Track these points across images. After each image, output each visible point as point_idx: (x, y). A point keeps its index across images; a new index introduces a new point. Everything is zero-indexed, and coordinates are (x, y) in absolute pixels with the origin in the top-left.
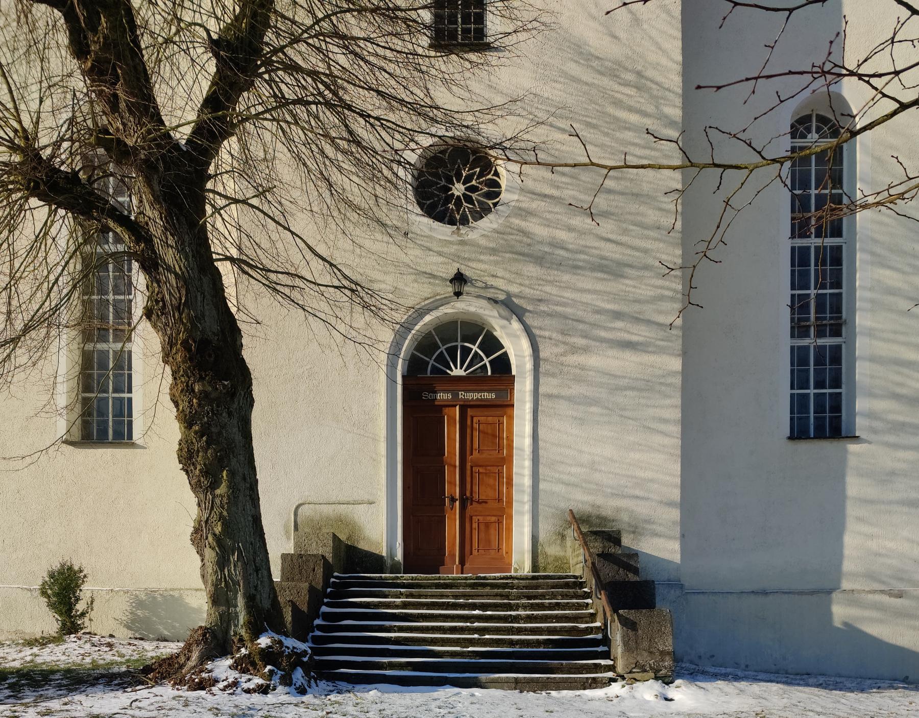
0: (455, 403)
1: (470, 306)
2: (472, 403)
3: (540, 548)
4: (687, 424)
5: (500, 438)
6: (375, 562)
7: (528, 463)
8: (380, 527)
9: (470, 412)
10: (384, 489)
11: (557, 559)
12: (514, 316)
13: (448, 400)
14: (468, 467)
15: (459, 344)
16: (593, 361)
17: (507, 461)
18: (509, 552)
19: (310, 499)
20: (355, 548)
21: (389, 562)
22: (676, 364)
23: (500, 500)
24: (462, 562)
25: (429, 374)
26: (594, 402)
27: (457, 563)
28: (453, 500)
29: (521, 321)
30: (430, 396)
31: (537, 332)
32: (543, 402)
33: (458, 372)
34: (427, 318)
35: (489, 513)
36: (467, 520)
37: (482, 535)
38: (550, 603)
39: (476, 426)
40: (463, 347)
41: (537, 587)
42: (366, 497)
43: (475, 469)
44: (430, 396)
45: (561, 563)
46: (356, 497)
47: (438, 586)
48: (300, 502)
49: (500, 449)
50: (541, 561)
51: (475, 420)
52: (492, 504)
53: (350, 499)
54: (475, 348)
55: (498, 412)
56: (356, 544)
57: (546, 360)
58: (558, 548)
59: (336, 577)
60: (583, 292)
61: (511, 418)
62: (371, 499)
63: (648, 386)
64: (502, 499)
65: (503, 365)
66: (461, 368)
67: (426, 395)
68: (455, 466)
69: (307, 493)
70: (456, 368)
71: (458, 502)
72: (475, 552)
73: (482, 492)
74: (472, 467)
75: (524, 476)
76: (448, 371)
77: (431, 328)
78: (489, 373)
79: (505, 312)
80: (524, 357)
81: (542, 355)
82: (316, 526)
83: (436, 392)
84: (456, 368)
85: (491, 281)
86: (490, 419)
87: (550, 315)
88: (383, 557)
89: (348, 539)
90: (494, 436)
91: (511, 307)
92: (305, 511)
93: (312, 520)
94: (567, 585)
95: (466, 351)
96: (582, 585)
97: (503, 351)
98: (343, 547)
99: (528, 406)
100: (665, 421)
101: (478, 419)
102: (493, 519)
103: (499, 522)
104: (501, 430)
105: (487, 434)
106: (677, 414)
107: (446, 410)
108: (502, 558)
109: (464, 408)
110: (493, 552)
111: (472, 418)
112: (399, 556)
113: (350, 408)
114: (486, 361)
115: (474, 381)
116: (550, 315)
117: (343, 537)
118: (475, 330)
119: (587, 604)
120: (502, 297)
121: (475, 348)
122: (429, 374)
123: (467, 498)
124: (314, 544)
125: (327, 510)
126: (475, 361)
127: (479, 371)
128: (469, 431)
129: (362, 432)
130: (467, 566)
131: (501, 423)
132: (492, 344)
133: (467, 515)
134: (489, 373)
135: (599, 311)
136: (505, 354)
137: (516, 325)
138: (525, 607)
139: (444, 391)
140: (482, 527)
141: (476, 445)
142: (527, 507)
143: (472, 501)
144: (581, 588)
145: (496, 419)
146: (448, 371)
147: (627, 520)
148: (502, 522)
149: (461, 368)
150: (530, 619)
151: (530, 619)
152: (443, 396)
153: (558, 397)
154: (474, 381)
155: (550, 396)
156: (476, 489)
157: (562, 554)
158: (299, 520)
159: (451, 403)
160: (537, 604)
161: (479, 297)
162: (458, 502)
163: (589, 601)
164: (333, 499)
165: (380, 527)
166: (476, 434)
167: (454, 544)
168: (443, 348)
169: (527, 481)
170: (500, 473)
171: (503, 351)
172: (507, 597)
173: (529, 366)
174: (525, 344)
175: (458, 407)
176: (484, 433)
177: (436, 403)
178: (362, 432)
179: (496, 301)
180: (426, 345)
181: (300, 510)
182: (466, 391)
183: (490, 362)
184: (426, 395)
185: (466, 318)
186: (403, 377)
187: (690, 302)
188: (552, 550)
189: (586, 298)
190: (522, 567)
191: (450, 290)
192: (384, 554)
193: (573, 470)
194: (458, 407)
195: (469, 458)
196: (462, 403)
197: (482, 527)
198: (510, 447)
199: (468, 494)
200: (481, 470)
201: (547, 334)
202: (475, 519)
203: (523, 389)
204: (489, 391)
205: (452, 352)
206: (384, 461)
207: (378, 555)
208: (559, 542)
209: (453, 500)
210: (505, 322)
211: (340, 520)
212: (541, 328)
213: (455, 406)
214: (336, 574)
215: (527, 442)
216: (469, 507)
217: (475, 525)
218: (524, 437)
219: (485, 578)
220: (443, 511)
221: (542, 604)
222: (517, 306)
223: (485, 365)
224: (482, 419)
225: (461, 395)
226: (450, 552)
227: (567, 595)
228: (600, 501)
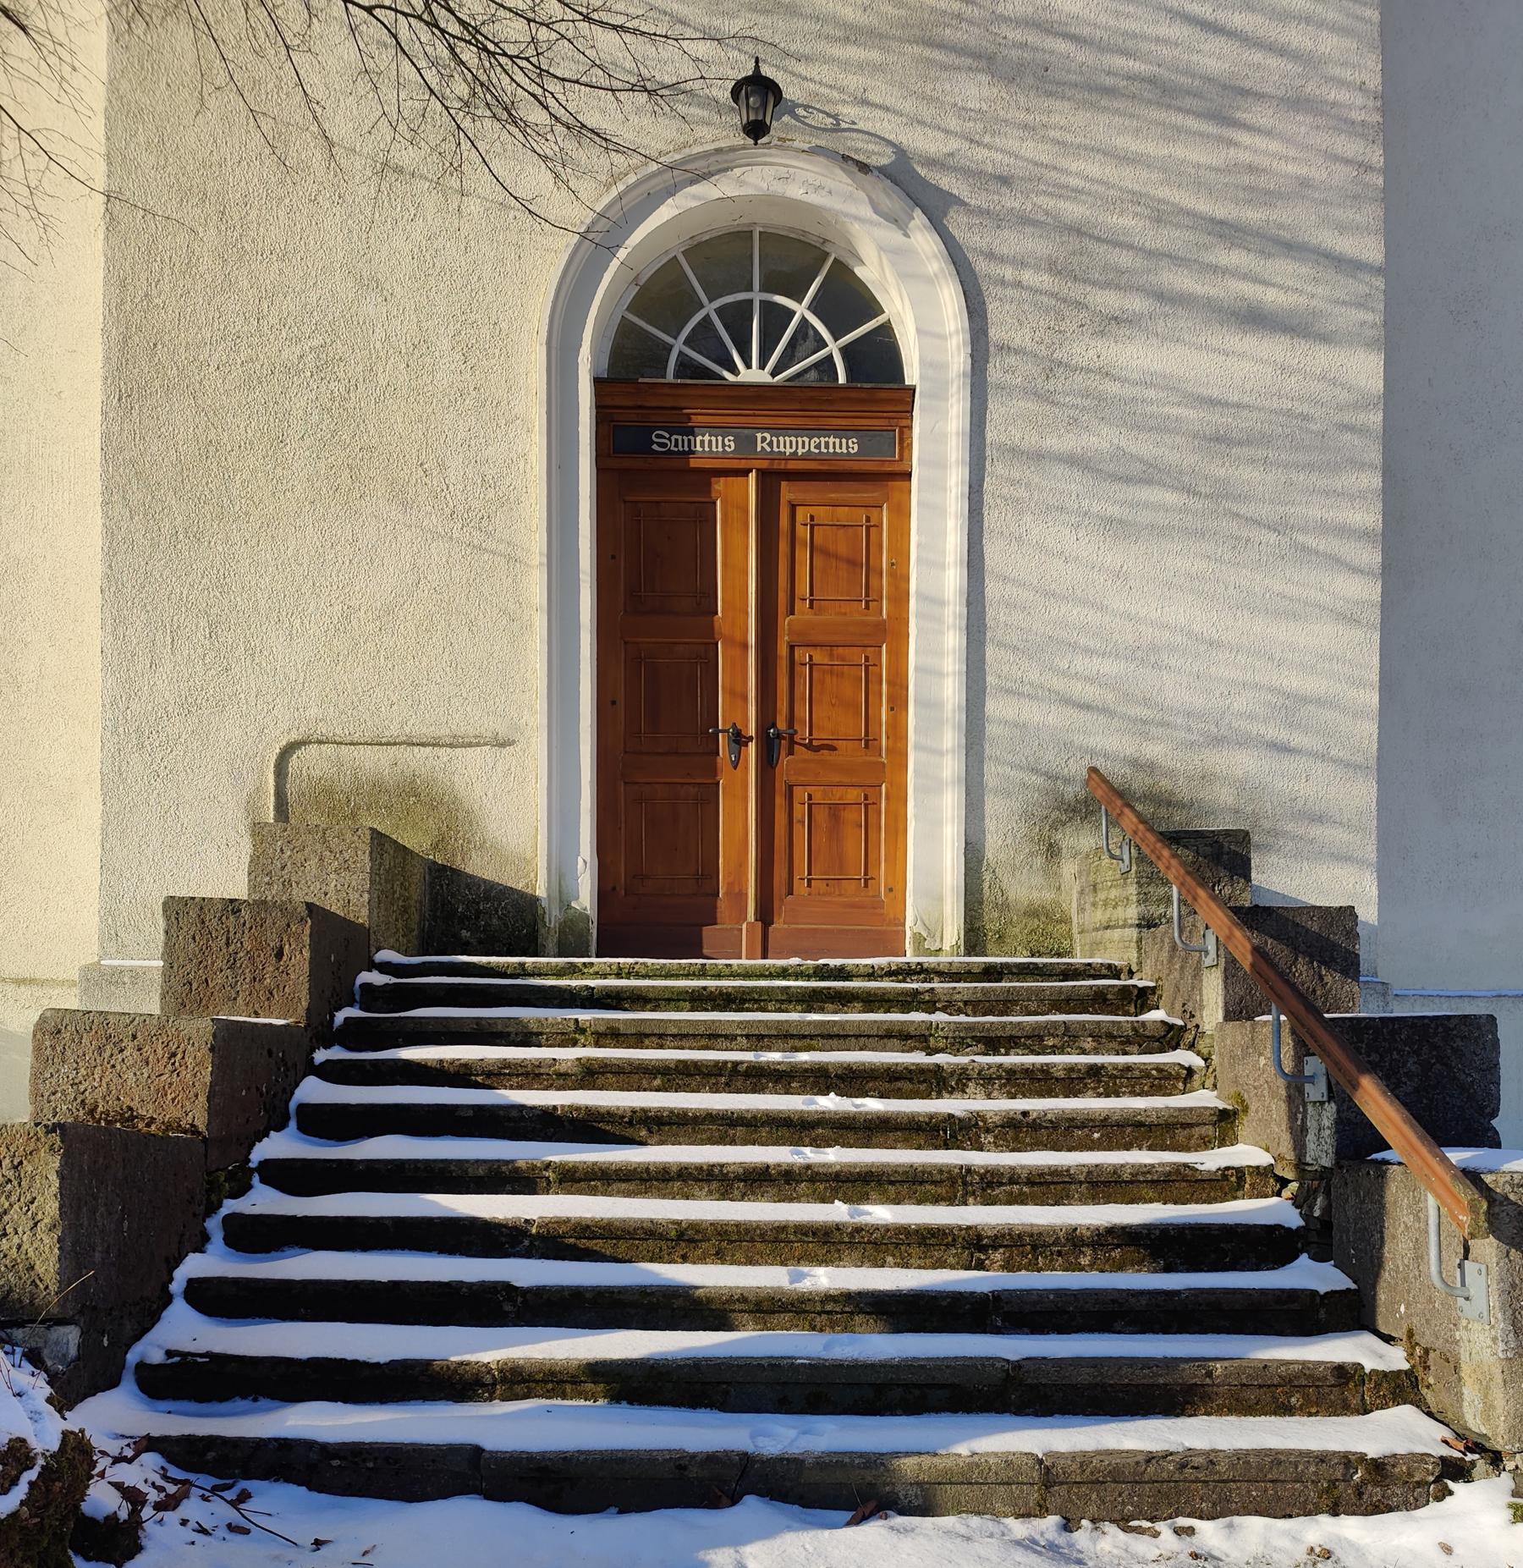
0: (743, 464)
1: (785, 182)
2: (792, 465)
3: (987, 877)
4: (1397, 535)
5: (873, 570)
6: (512, 921)
7: (954, 640)
8: (530, 820)
9: (788, 492)
10: (541, 705)
11: (1033, 912)
12: (918, 212)
13: (724, 456)
14: (783, 650)
15: (757, 296)
16: (1135, 355)
17: (893, 632)
18: (897, 890)
19: (323, 729)
20: (457, 873)
21: (553, 917)
22: (1366, 370)
23: (870, 742)
24: (765, 915)
25: (670, 377)
26: (1151, 474)
27: (751, 916)
28: (739, 739)
29: (938, 226)
30: (676, 442)
31: (981, 266)
32: (996, 470)
33: (753, 375)
34: (665, 213)
35: (840, 780)
36: (780, 801)
37: (820, 839)
38: (1071, 1069)
39: (803, 532)
40: (769, 309)
41: (1005, 1005)
42: (489, 725)
43: (802, 655)
44: (676, 442)
45: (1046, 917)
46: (459, 724)
47: (699, 1000)
48: (295, 736)
49: (871, 599)
50: (991, 920)
51: (801, 514)
52: (848, 752)
53: (443, 732)
54: (801, 310)
55: (867, 494)
56: (458, 864)
57: (1003, 348)
58: (1038, 880)
59: (385, 968)
60: (1107, 164)
61: (902, 513)
62: (503, 732)
63: (1294, 439)
64: (878, 740)
65: (878, 361)
66: (762, 367)
67: (663, 440)
68: (745, 646)
69: (313, 712)
70: (748, 366)
71: (752, 746)
72: (801, 887)
73: (820, 716)
74: (792, 648)
75: (941, 675)
76: (727, 375)
77: (675, 247)
78: (842, 379)
79: (893, 201)
80: (943, 337)
81: (995, 334)
82: (338, 803)
83: (691, 432)
84: (748, 366)
85: (849, 112)
86: (842, 511)
87: (1025, 221)
88: (534, 901)
89: (435, 847)
90: (853, 563)
91: (908, 186)
92: (306, 762)
93: (329, 792)
94: (1098, 1001)
95: (776, 319)
96: (1143, 999)
97: (880, 320)
98: (417, 874)
99: (956, 479)
100: (1343, 531)
101: (809, 509)
102: (853, 795)
103: (870, 804)
104: (873, 547)
105: (837, 557)
106: (1369, 517)
107: (719, 485)
108: (877, 904)
109: (772, 478)
110: (850, 887)
111: (793, 508)
112: (585, 898)
113: (442, 466)
114: (833, 348)
115: (803, 401)
116: (1025, 221)
117: (416, 840)
118: (801, 260)
119: (1190, 1071)
120: (884, 158)
121: (801, 310)
122: (670, 377)
123: (778, 736)
124: (314, 862)
125: (375, 762)
126: (801, 350)
127: (813, 375)
128: (783, 546)
129: (477, 538)
130: (778, 925)
131: (872, 527)
132: (848, 301)
133: (780, 787)
134: (842, 379)
135: (1161, 215)
136: (886, 329)
137: (925, 242)
138: (989, 1081)
139: (713, 428)
140: (821, 816)
141: (803, 588)
142: (951, 767)
143: (792, 742)
144: (1144, 1007)
145: (862, 514)
146: (727, 375)
147: (1230, 801)
148: (877, 803)
149: (762, 367)
150: (1018, 1132)
151: (1018, 1132)
152: (710, 445)
153: (1038, 457)
154: (803, 401)
155: (1014, 452)
156: (803, 711)
157: (1048, 896)
158: (291, 788)
159: (735, 464)
160: (1028, 1072)
161: (816, 151)
162: (752, 746)
163: (1182, 1057)
164: (393, 731)
165: (530, 820)
166: (803, 556)
167: (743, 864)
168: (710, 308)
169: (951, 691)
170: (871, 665)
171: (880, 320)
172: (920, 1039)
173: (958, 358)
174: (950, 298)
175: (752, 476)
176: (826, 553)
177: (694, 463)
178: (477, 538)
179: (864, 168)
180: (661, 295)
181: (294, 761)
182: (776, 430)
183: (845, 351)
184: (663, 440)
185: (778, 221)
186: (597, 382)
187: (1402, 202)
188: (1022, 886)
189: (1129, 178)
190: (935, 930)
191: (725, 131)
192: (541, 892)
193: (1095, 665)
194: (752, 476)
195: (785, 622)
196: (764, 465)
197: (821, 816)
198: (900, 598)
199: (782, 725)
200: (819, 657)
201: (1009, 273)
202: (800, 794)
203: (937, 436)
204: (840, 432)
205: (737, 319)
206: (540, 622)
207: (521, 894)
208: (1039, 861)
209: (739, 739)
210: (892, 236)
211: (414, 794)
212: (991, 256)
213: (745, 473)
214: (385, 955)
215: (953, 580)
216: (785, 761)
217: (800, 811)
218: (942, 566)
219: (842, 974)
220: (713, 771)
221: (1045, 1070)
222: (924, 182)
223: (830, 357)
224: (821, 513)
225: (764, 441)
226: (730, 885)
227: (1111, 1037)
228: (1154, 751)
